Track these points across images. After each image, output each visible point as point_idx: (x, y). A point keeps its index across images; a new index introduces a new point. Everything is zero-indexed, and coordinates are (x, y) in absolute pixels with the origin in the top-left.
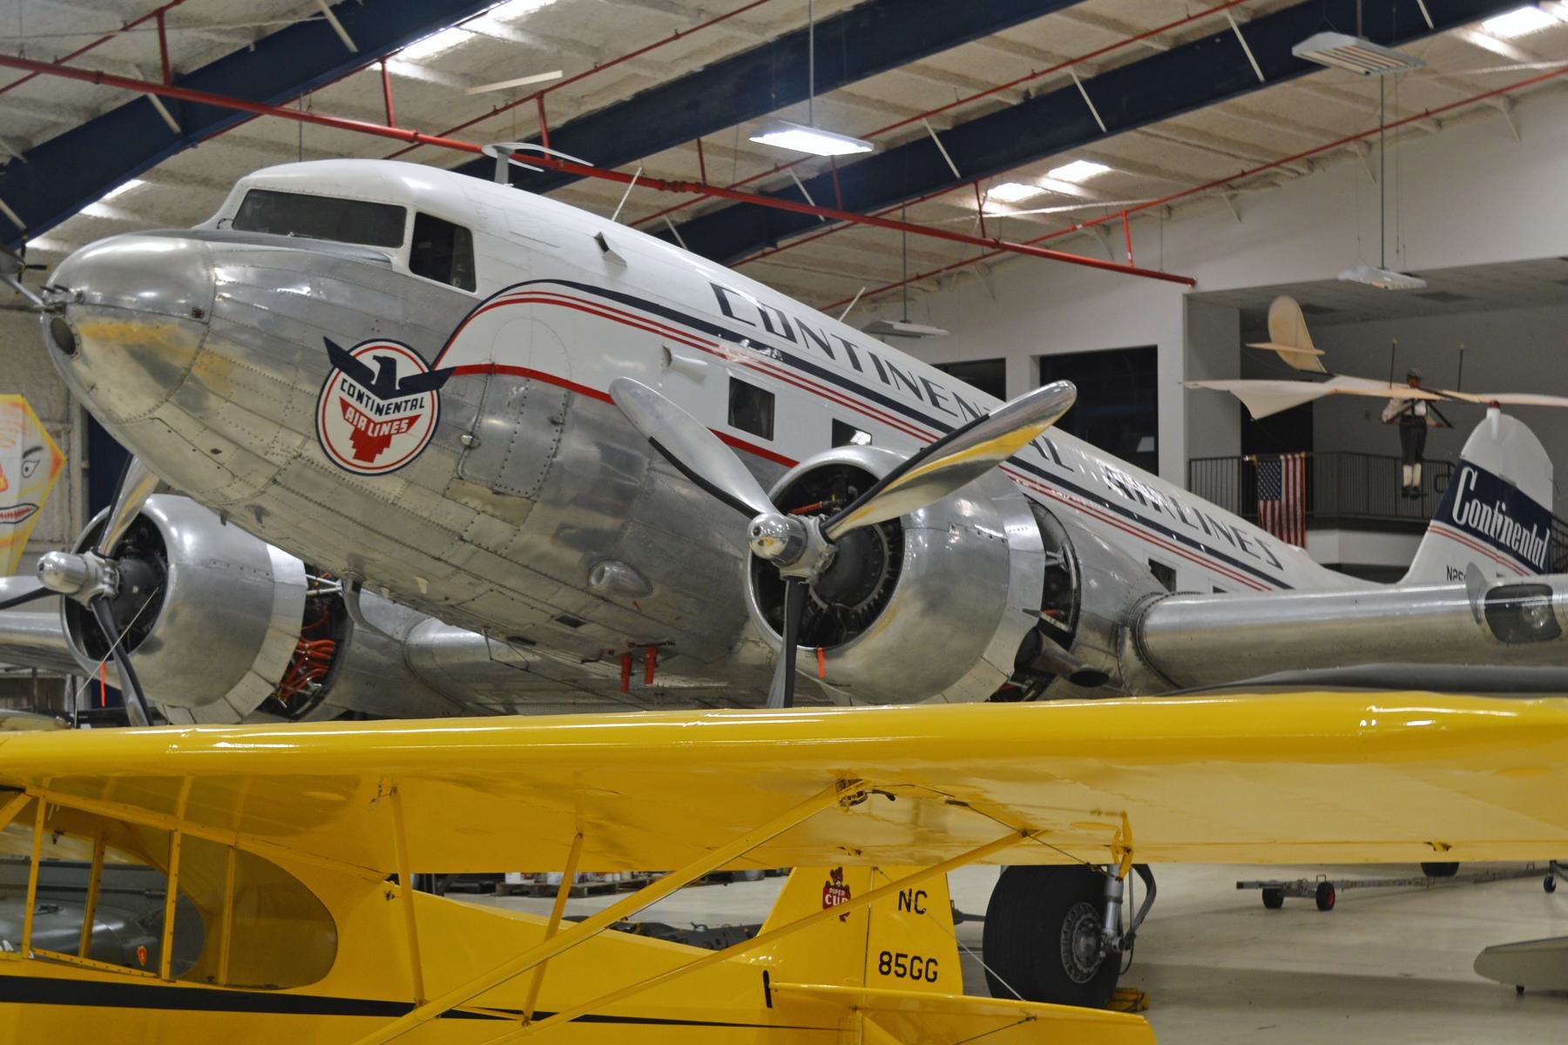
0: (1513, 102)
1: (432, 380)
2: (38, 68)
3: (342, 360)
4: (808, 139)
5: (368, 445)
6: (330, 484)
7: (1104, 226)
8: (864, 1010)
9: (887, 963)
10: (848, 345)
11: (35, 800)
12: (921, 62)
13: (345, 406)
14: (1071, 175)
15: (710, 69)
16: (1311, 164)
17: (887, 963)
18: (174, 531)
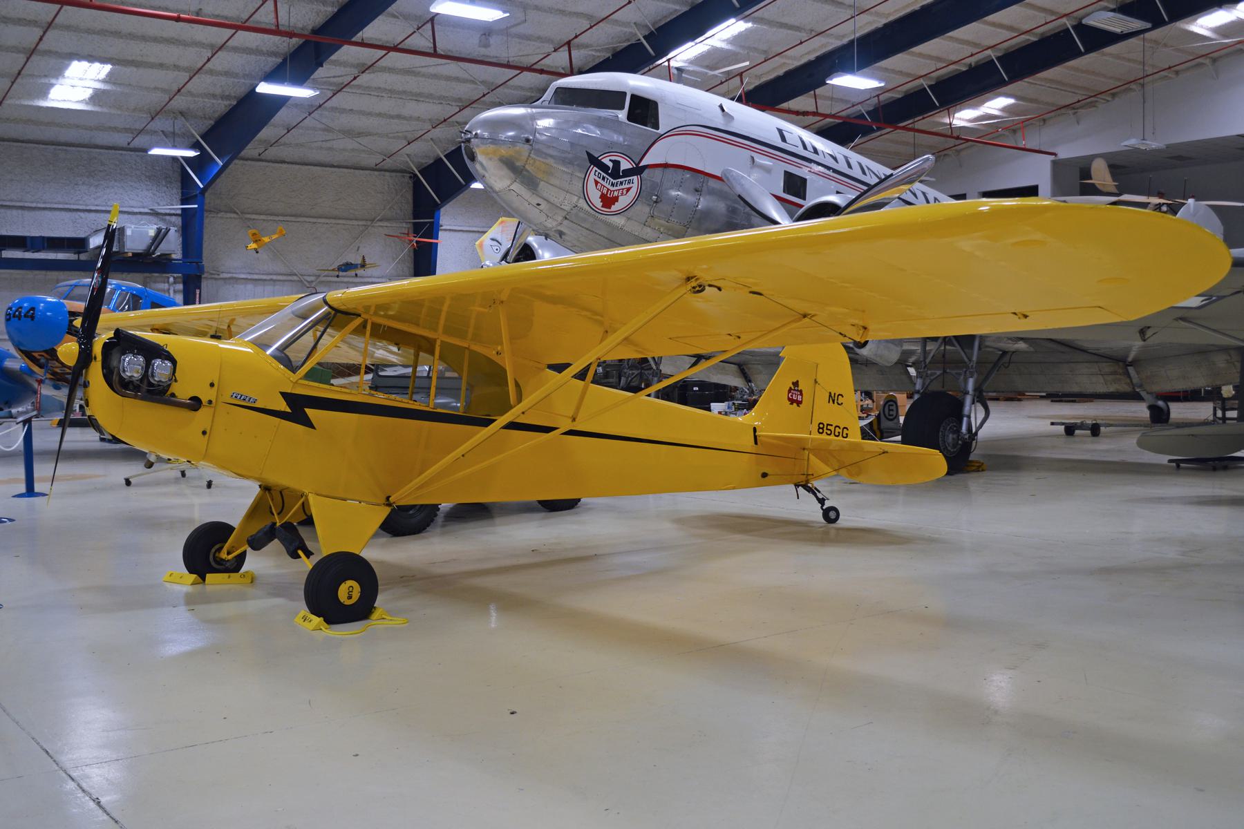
0: (1214, 60)
1: (638, 170)
2: (523, 69)
3: (595, 161)
4: (856, 83)
5: (608, 201)
6: (591, 219)
7: (1013, 129)
8: (810, 450)
9: (821, 428)
10: (846, 158)
11: (366, 321)
12: (916, 49)
13: (597, 183)
14: (996, 105)
15: (818, 58)
16: (1114, 95)
17: (821, 428)
18: (540, 252)
